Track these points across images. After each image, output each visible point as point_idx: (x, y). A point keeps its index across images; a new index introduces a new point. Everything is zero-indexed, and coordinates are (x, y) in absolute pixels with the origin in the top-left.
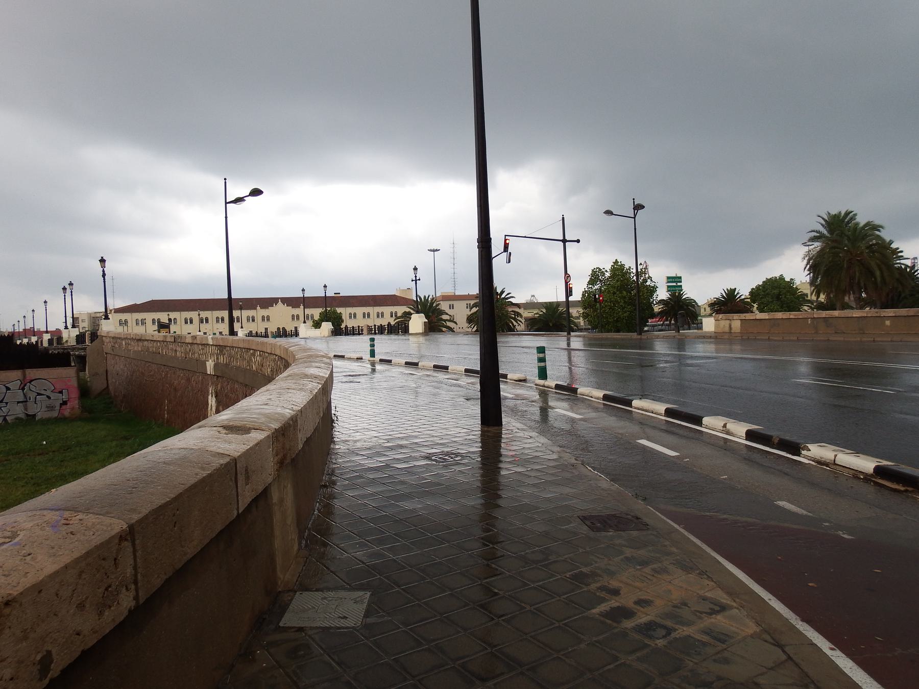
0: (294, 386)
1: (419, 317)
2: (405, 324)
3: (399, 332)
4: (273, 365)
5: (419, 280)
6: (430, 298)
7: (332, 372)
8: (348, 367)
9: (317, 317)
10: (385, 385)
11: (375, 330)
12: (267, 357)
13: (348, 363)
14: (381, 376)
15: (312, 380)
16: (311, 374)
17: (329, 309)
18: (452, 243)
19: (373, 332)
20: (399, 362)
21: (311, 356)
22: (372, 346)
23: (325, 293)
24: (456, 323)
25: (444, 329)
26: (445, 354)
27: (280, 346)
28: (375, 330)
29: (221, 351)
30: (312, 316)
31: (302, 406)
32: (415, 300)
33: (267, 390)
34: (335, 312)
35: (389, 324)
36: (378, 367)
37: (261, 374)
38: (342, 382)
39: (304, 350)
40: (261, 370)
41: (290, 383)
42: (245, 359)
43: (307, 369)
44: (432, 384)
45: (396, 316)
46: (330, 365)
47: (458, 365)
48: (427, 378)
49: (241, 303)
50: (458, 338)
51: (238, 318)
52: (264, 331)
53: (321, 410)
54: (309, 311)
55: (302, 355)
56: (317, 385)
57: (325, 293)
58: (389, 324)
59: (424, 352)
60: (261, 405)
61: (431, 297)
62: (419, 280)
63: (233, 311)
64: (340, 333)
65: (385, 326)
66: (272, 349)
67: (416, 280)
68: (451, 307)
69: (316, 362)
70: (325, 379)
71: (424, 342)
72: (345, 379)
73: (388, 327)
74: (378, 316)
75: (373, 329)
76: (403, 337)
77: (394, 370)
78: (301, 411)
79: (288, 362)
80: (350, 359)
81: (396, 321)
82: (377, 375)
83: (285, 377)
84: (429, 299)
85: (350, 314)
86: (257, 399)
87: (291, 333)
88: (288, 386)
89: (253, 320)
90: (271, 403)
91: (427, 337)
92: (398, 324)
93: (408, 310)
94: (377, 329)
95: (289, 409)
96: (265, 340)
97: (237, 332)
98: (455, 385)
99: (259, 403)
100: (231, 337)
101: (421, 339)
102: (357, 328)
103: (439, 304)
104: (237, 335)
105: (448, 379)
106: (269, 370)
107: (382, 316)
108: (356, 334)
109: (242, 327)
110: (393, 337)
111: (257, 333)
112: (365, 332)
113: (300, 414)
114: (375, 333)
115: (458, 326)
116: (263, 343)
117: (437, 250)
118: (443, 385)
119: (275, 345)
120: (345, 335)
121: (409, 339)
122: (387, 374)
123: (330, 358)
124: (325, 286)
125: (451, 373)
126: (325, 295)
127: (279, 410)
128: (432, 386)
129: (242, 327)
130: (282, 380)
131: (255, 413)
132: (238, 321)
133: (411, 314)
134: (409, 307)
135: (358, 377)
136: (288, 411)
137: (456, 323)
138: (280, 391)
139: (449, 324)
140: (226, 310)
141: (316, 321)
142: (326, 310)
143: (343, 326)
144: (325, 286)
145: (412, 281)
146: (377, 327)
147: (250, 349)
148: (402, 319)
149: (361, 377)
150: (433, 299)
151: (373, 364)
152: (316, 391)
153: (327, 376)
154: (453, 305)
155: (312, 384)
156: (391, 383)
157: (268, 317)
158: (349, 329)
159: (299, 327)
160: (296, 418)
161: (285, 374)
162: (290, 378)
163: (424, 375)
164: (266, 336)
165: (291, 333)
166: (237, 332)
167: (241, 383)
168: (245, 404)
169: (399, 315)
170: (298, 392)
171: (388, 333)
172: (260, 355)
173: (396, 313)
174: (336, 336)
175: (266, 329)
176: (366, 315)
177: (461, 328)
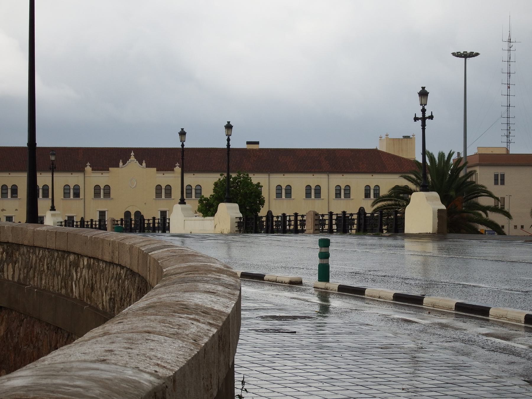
0: (159, 328)
1: (427, 199)
2: (397, 212)
3: (381, 231)
4: (115, 287)
5: (431, 117)
6: (453, 158)
7: (238, 308)
8: (270, 300)
9: (208, 192)
10: (347, 340)
11: (331, 225)
12: (102, 271)
13: (271, 292)
14: (341, 321)
15: (197, 317)
16: (196, 305)
17: (234, 175)
18: (506, 38)
19: (327, 227)
20: (382, 294)
21: (195, 270)
22: (325, 256)
23: (228, 140)
24: (507, 215)
25: (481, 228)
26: (481, 280)
27: (131, 247)
28: (331, 225)
29: (10, 256)
30: (199, 189)
31: (177, 369)
32: (420, 160)
33: (105, 334)
34: (247, 183)
35: (361, 211)
36: (335, 303)
37: (90, 306)
38: (256, 331)
39: (180, 256)
40: (89, 297)
41: (151, 321)
42: (58, 274)
43: (187, 295)
44: (452, 344)
45: (376, 195)
46: (238, 290)
47: (509, 306)
48: (441, 332)
49: (53, 158)
50: (512, 248)
51: (45, 189)
52: (97, 218)
53: (215, 381)
54: (191, 179)
55: (177, 266)
56: (208, 327)
57: (228, 140)
58: (361, 211)
59: (436, 275)
60: (92, 362)
61: (455, 156)
62: (431, 117)
63: (38, 175)
64: (256, 227)
65: (352, 215)
66: (113, 252)
67: (424, 119)
68: (500, 180)
69: (207, 282)
70: (224, 318)
71: (436, 252)
72: (264, 325)
73: (359, 218)
74: (338, 195)
75: (327, 222)
76: (390, 242)
77: (368, 311)
78: (173, 379)
79: (146, 282)
80: (275, 283)
81: (376, 207)
82: (332, 320)
83: (143, 309)
84: (451, 161)
85: (279, 188)
86: (84, 349)
87: (154, 223)
88: (147, 327)
89: (77, 195)
90: (112, 358)
91: (443, 244)
92: (381, 214)
93: (403, 182)
94: (334, 222)
95: (148, 373)
96: (101, 234)
97: (43, 217)
98: (504, 350)
99: (87, 357)
100: (31, 227)
101: (431, 247)
102: (292, 218)
103: (471, 173)
104: (42, 223)
105: (487, 335)
106: (106, 298)
107: (348, 195)
108: (290, 232)
109: (53, 209)
110: (369, 240)
111: (82, 221)
112: (309, 226)
113: (170, 385)
114: (331, 231)
115: (513, 222)
116: (95, 241)
117: (472, 55)
118: (473, 348)
119: (121, 245)
120: (267, 232)
121: (403, 247)
122: (355, 317)
123: (234, 275)
124: (229, 127)
125: (494, 323)
126: (228, 145)
127: (129, 374)
128: (452, 349)
129: (53, 209)
130: (135, 314)
131: (80, 377)
132: (45, 195)
133: (411, 192)
134: (405, 177)
135: (292, 321)
136: (147, 376)
137: (507, 215)
138: (130, 335)
139: (493, 217)
140: (39, 148)
141: (206, 199)
142: (229, 177)
143: (263, 213)
144: (229, 127)
145: (416, 119)
146: (334, 217)
147: (69, 253)
148: (389, 202)
149: (299, 321)
150: (459, 160)
151: (324, 295)
152: (206, 340)
153: (229, 311)
154: (503, 176)
155: (197, 327)
156: (364, 339)
157: (107, 189)
158: (275, 219)
159: (171, 211)
160: (164, 393)
161: (142, 303)
162: (151, 311)
163: (434, 324)
164: (102, 226)
165: (154, 223)
166: (43, 217)
167: (48, 324)
168: (59, 359)
169: (384, 192)
170: (169, 340)
171: (358, 231)
172: (89, 267)
173: (377, 188)
174: (248, 233)
175: (102, 214)
176: (313, 192)
177: (519, 227)
